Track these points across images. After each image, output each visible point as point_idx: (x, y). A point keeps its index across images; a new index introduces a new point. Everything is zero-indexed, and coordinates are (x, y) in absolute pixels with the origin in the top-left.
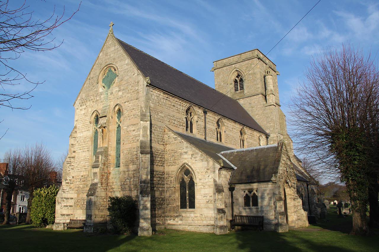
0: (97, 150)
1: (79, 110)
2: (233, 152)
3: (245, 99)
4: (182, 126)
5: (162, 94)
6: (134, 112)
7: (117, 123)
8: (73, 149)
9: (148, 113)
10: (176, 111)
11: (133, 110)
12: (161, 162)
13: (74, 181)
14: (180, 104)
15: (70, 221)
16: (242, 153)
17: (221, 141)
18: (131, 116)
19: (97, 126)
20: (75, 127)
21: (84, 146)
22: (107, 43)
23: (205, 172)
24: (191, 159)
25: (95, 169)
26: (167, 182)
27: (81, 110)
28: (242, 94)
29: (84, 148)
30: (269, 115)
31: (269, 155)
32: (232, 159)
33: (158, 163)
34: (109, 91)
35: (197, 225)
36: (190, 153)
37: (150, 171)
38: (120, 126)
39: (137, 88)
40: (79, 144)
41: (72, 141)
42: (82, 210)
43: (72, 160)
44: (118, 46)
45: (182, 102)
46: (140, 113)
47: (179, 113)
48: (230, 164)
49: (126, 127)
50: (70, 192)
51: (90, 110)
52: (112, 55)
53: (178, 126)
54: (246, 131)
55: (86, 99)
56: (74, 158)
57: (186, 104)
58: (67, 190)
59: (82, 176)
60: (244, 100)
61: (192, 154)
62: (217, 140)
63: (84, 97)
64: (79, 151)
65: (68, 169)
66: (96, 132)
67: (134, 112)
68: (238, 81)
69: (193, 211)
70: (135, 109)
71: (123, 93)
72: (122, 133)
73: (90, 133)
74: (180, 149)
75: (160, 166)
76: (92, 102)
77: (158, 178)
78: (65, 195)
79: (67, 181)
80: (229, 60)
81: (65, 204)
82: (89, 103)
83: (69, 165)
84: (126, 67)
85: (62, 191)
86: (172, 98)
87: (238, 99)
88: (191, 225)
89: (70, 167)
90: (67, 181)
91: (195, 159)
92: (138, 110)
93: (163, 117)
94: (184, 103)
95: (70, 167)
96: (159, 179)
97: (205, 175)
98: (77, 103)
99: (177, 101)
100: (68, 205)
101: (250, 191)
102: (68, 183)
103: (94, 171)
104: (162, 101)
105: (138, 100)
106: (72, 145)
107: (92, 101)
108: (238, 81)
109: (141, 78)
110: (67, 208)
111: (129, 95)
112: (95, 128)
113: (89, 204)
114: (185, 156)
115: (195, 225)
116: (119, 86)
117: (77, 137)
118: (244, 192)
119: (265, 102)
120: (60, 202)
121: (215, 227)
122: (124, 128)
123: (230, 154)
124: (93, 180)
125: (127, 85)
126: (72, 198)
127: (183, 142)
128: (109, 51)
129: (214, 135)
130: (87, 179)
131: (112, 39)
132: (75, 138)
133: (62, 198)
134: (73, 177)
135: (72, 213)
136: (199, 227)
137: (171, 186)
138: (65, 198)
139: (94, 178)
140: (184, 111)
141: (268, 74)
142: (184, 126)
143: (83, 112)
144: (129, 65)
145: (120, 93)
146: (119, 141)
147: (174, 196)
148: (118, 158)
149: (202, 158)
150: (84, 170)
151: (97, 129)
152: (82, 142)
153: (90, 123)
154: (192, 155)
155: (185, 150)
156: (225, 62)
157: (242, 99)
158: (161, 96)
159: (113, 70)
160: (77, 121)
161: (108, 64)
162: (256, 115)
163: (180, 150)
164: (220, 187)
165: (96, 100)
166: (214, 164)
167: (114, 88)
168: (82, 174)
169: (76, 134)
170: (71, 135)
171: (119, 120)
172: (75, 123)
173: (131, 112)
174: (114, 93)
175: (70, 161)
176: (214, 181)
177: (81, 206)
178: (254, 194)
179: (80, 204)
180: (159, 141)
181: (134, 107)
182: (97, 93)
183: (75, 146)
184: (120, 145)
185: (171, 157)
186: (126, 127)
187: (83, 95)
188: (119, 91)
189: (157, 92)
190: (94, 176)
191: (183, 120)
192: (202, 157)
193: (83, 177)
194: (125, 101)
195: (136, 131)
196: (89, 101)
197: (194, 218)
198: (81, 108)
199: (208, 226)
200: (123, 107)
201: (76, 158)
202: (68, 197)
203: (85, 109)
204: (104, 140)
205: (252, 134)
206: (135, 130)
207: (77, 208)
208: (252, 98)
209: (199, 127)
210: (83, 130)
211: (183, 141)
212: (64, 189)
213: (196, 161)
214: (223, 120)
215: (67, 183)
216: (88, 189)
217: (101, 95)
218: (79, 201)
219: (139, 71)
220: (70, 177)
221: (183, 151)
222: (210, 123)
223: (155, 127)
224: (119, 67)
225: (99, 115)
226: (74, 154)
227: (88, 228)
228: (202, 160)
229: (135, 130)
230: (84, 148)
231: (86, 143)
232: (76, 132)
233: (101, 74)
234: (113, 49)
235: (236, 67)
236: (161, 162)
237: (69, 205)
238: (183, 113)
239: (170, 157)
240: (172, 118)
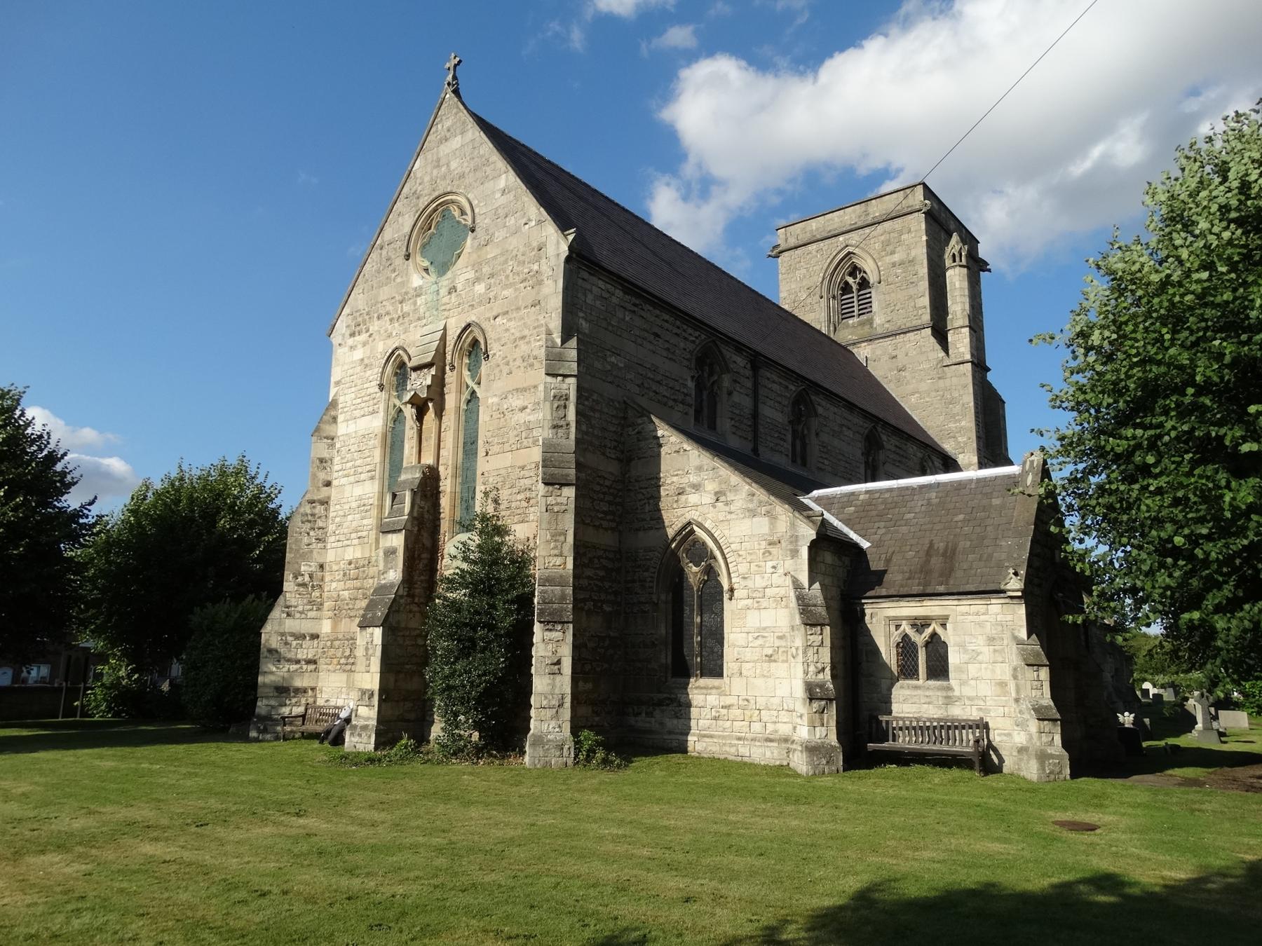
0: (399, 476)
1: (345, 349)
2: (853, 494)
3: (877, 344)
4: (681, 405)
5: (619, 293)
6: (524, 348)
8: (322, 476)
9: (570, 351)
10: (665, 354)
11: (522, 342)
12: (612, 517)
14: (678, 331)
15: (306, 710)
16: (887, 495)
17: (804, 464)
18: (515, 360)
19: (399, 397)
20: (334, 404)
21: (359, 462)
22: (440, 126)
23: (762, 551)
24: (714, 507)
25: (390, 536)
26: (630, 585)
27: (351, 347)
28: (867, 328)
29: (360, 470)
30: (956, 394)
31: (991, 505)
32: (850, 514)
33: (601, 519)
34: (445, 282)
35: (730, 737)
36: (711, 487)
37: (572, 543)
38: (478, 395)
39: (536, 267)
40: (342, 458)
41: (320, 449)
43: (319, 509)
44: (473, 134)
45: (685, 327)
46: (543, 350)
47: (674, 361)
48: (846, 530)
49: (495, 400)
50: (310, 614)
51: (382, 348)
52: (454, 165)
53: (671, 403)
54: (884, 438)
55: (368, 314)
56: (327, 503)
57: (697, 334)
58: (300, 608)
59: (350, 563)
60: (874, 346)
61: (717, 490)
62: (794, 461)
63: (361, 307)
64: (344, 481)
65: (306, 540)
66: (398, 416)
67: (524, 348)
68: (855, 287)
69: (717, 688)
70: (527, 340)
71: (489, 288)
72: (483, 417)
73: (377, 423)
74: (677, 475)
75: (606, 529)
76: (388, 323)
77: (597, 569)
78: (291, 625)
80: (828, 220)
82: (376, 323)
83: (309, 525)
84: (501, 200)
85: (283, 612)
86: (651, 308)
87: (854, 344)
88: (711, 737)
89: (312, 533)
91: (727, 509)
92: (539, 341)
93: (620, 369)
94: (690, 331)
95: (312, 533)
96: (602, 573)
97: (763, 564)
98: (341, 326)
99: (667, 321)
100: (299, 656)
101: (920, 624)
102: (304, 585)
103: (388, 544)
104: (620, 314)
105: (538, 307)
106: (322, 460)
107: (387, 318)
108: (855, 287)
109: (550, 230)
112: (395, 406)
113: (367, 654)
114: (693, 498)
115: (724, 737)
116: (477, 266)
118: (898, 627)
119: (942, 354)
121: (794, 746)
122: (490, 401)
123: (845, 499)
124: (383, 574)
125: (503, 259)
127: (685, 450)
128: (445, 149)
129: (782, 443)
130: (364, 571)
131: (455, 110)
133: (282, 634)
135: (313, 685)
136: (736, 742)
137: (643, 599)
138: (292, 635)
139: (385, 566)
140: (688, 356)
141: (954, 261)
142: (690, 406)
143: (359, 354)
144: (509, 192)
145: (480, 288)
146: (474, 446)
147: (653, 632)
149: (751, 506)
150: (355, 542)
151: (402, 407)
152: (353, 450)
153: (381, 387)
154: (716, 493)
155: (693, 478)
156: (814, 228)
157: (866, 344)
158: (614, 300)
159: (457, 213)
160: (338, 383)
161: (441, 192)
162: (913, 394)
163: (675, 479)
164: (815, 606)
165: (399, 312)
166: (793, 525)
167: (462, 272)
170: (317, 430)
171: (473, 377)
172: (333, 392)
173: (515, 347)
174: (459, 287)
175: (313, 515)
176: (793, 582)
177: (343, 661)
178: (934, 635)
179: (339, 655)
180: (605, 446)
181: (526, 332)
182: (404, 290)
183: (329, 464)
184: (476, 457)
185: (646, 501)
186: (495, 400)
187: (358, 299)
188: (477, 280)
189: (601, 284)
190: (386, 562)
191: (685, 386)
192: (751, 501)
193: (353, 566)
194: (495, 313)
195: (528, 410)
196: (379, 318)
197: (721, 710)
198: (350, 341)
199: (771, 741)
200: (491, 335)
201: (331, 503)
202: (302, 632)
203: (364, 344)
205: (900, 448)
206: (525, 408)
207: (330, 667)
208: (900, 338)
209: (737, 412)
210: (357, 413)
211: (686, 446)
212: (288, 603)
213: (730, 513)
214: (813, 398)
215: (299, 585)
216: (364, 604)
217: (418, 295)
218: (336, 643)
219: (542, 209)
220: (310, 566)
221: (685, 480)
222: (772, 402)
223: (593, 400)
224: (476, 202)
225: (410, 359)
226: (325, 492)
227: (360, 735)
228: (753, 513)
229: (525, 408)
230: (360, 470)
231: (366, 456)
234: (456, 142)
235: (850, 242)
236: (612, 517)
237: (304, 657)
238: (686, 363)
239: (643, 502)
240: (650, 375)
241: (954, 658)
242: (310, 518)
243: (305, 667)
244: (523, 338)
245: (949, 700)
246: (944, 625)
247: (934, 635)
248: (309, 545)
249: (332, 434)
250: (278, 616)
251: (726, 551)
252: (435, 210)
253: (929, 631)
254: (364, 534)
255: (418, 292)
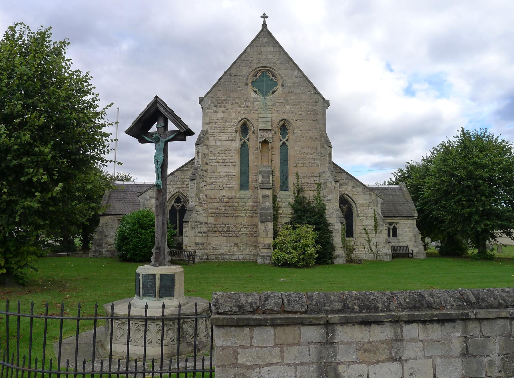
6: (310, 134)
7: (281, 140)
13: (207, 201)
18: (307, 137)
24: (352, 190)
39: (314, 108)
42: (225, 238)
43: (205, 174)
58: (201, 212)
65: (201, 186)
79: (200, 201)
81: (199, 230)
89: (203, 183)
90: (200, 201)
95: (203, 183)
101: (391, 224)
102: (202, 203)
110: (201, 235)
111: (302, 113)
114: (345, 187)
117: (210, 145)
120: (193, 227)
126: (205, 223)
132: (207, 146)
133: (196, 222)
134: (206, 196)
135: (206, 242)
138: (199, 222)
143: (220, 115)
145: (288, 108)
148: (283, 180)
153: (236, 132)
168: (223, 193)
169: (208, 141)
175: (203, 176)
178: (394, 226)
186: (299, 148)
201: (208, 171)
204: (263, 157)
212: (197, 210)
215: (200, 203)
218: (218, 226)
232: (208, 138)
233: (251, 74)
241: (399, 232)
242: (202, 177)
243: (203, 235)
244: (310, 130)
245: (399, 242)
246: (396, 224)
247: (394, 226)
248: (202, 187)
249: (207, 144)
250: (194, 215)
251: (356, 203)
252: (260, 70)
253: (393, 225)
254: (231, 186)
255: (255, 100)
